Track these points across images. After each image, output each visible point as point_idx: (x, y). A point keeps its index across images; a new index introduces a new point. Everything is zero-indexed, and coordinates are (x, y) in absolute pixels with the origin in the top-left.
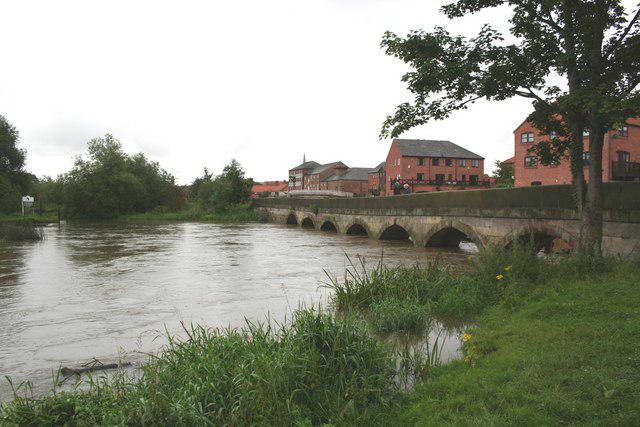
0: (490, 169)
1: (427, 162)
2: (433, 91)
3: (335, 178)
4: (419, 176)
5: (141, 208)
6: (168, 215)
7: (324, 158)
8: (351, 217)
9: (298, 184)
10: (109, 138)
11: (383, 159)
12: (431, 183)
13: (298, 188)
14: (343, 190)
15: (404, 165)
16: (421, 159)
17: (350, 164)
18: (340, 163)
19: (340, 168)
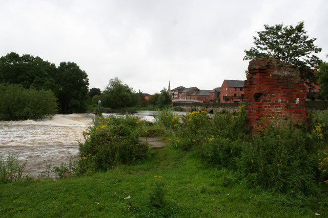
0: (90, 87)
1: (238, 89)
2: (53, 65)
3: (194, 94)
4: (235, 95)
5: (129, 106)
6: (142, 108)
7: (188, 85)
8: (221, 109)
9: (175, 96)
10: (116, 78)
11: (220, 86)
12: (239, 98)
13: (176, 98)
14: (198, 100)
15: (229, 90)
16: (236, 88)
17: (200, 89)
18: (196, 88)
19: (196, 90)
